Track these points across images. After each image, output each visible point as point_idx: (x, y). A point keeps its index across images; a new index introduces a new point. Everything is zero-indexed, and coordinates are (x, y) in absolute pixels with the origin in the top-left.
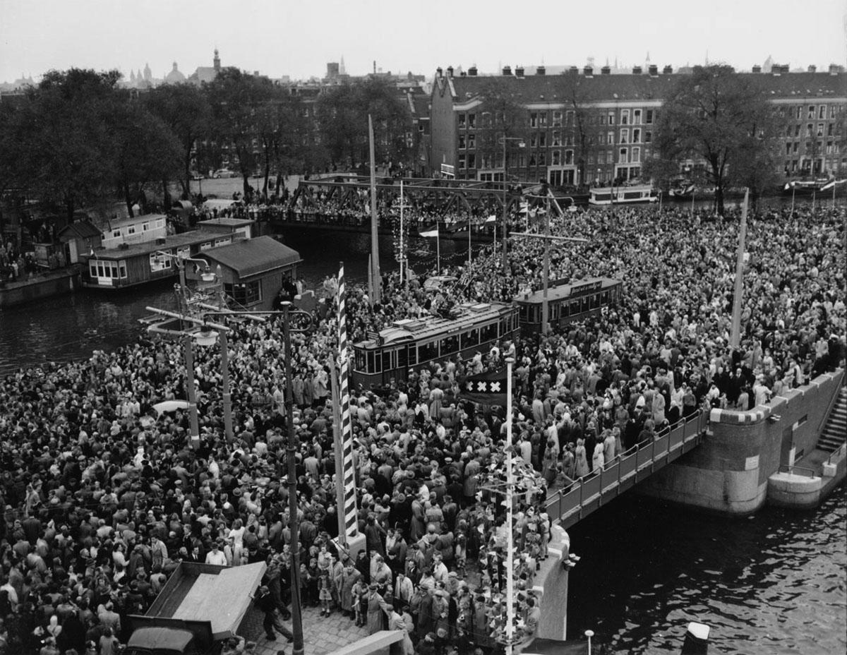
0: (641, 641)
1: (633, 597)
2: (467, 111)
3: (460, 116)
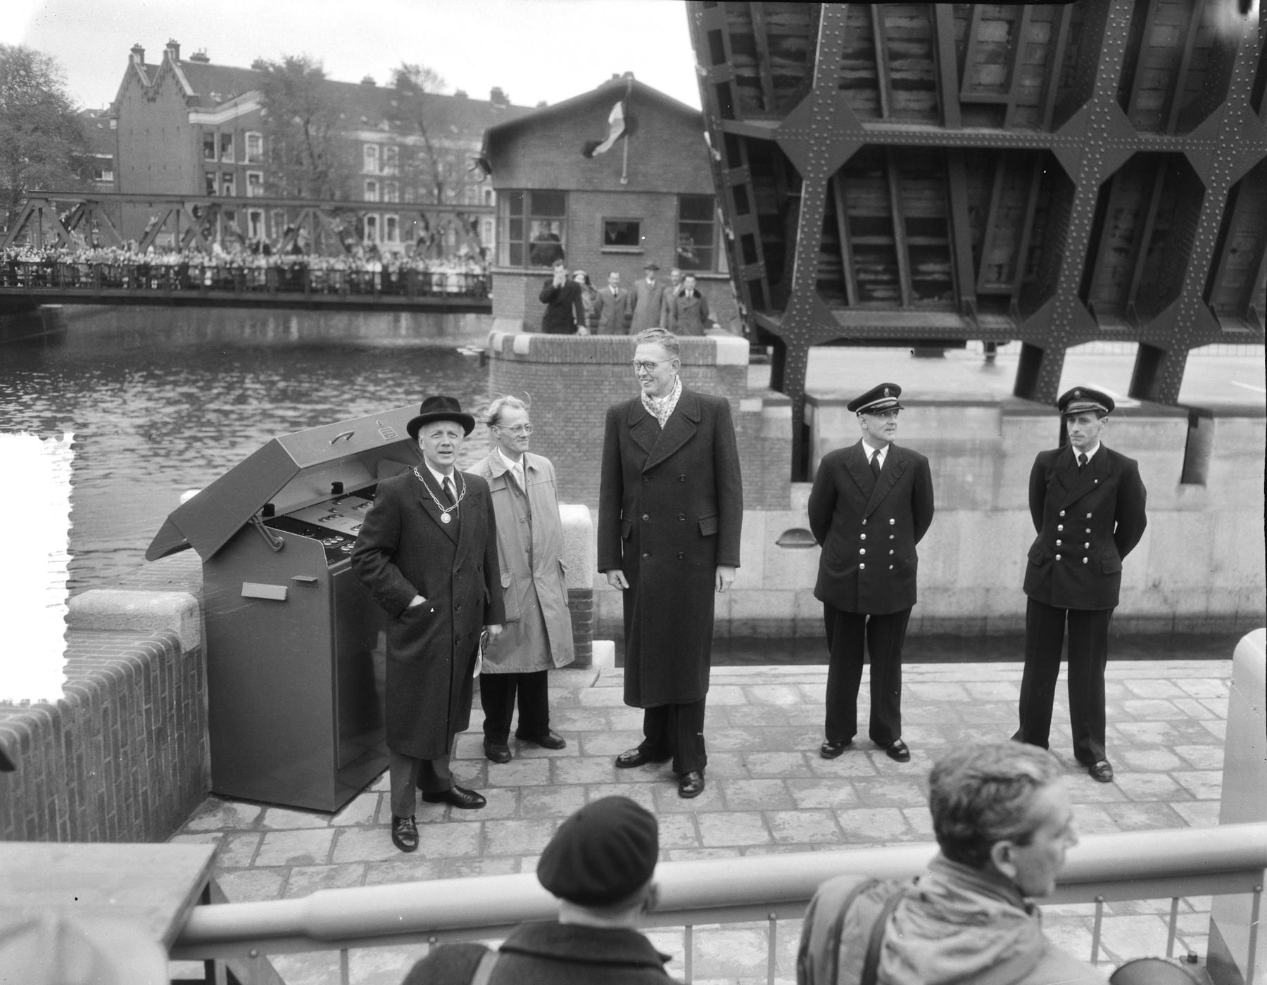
2: (218, 127)
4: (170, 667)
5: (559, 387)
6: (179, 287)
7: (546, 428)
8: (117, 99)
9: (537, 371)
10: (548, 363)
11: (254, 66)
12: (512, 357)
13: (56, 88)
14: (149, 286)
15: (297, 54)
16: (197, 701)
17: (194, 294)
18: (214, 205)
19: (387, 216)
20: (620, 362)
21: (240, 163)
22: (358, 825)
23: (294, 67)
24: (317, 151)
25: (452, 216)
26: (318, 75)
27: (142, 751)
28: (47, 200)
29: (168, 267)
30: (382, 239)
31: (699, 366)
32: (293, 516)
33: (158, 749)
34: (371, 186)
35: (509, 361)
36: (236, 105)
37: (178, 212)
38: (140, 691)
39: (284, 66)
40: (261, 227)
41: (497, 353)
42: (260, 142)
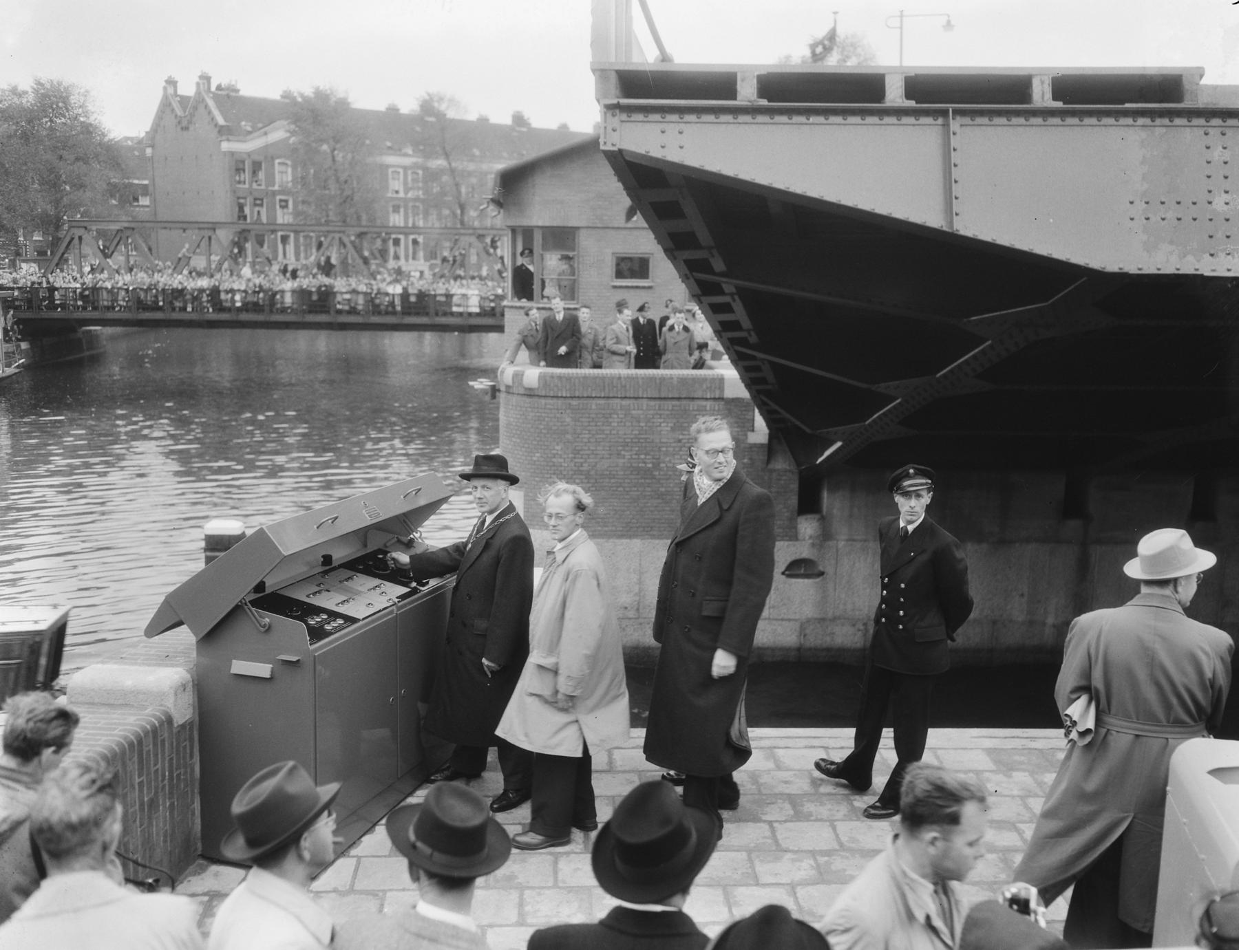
0: (833, 767)
1: (839, 444)
2: (249, 154)
3: (237, 161)
4: (163, 741)
5: (568, 420)
6: (211, 310)
7: (554, 460)
8: (151, 129)
9: (546, 404)
10: (557, 397)
11: (282, 97)
12: (522, 391)
13: (92, 120)
14: (184, 309)
15: (324, 85)
16: (189, 770)
17: (224, 316)
18: (244, 231)
19: (412, 237)
20: (628, 396)
21: (270, 188)
22: (335, 891)
23: (322, 96)
24: (343, 177)
25: (473, 239)
26: (343, 104)
27: (135, 821)
28: (86, 228)
29: (202, 291)
30: (407, 259)
31: (707, 399)
32: (281, 592)
33: (150, 818)
34: (396, 209)
35: (518, 394)
36: (266, 134)
37: (210, 238)
38: (133, 766)
39: (312, 95)
40: (290, 248)
41: (508, 387)
42: (290, 170)
